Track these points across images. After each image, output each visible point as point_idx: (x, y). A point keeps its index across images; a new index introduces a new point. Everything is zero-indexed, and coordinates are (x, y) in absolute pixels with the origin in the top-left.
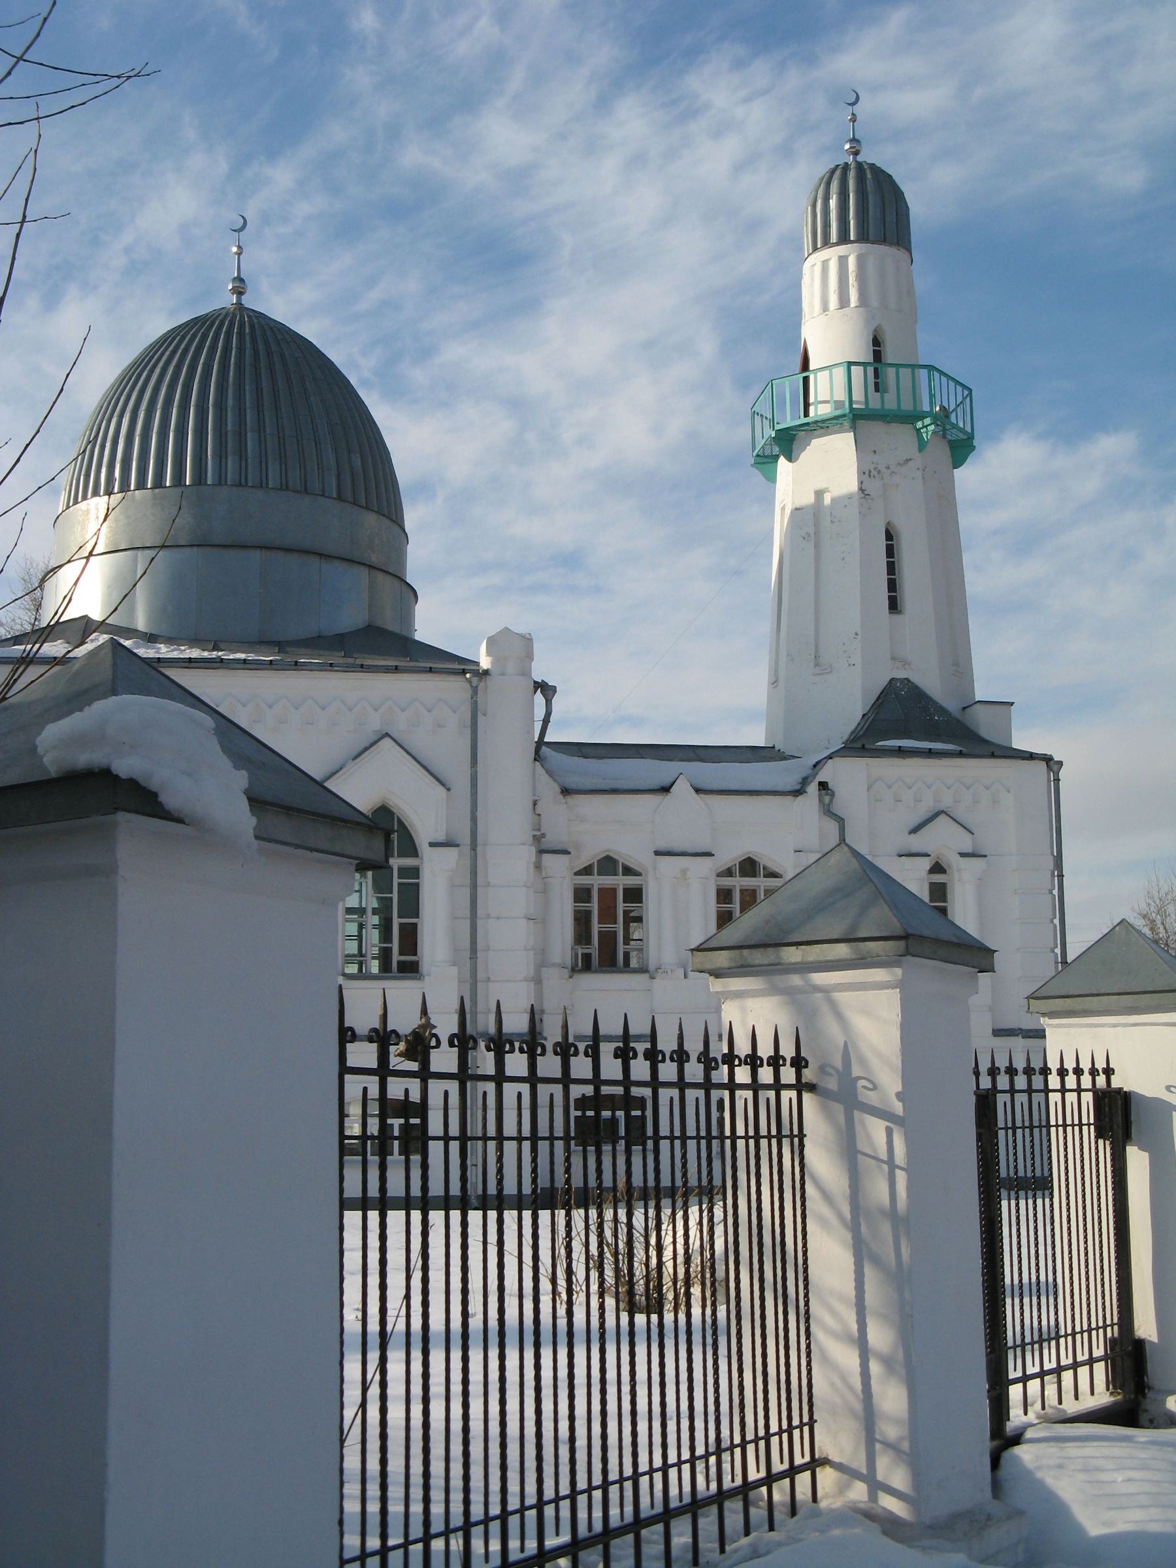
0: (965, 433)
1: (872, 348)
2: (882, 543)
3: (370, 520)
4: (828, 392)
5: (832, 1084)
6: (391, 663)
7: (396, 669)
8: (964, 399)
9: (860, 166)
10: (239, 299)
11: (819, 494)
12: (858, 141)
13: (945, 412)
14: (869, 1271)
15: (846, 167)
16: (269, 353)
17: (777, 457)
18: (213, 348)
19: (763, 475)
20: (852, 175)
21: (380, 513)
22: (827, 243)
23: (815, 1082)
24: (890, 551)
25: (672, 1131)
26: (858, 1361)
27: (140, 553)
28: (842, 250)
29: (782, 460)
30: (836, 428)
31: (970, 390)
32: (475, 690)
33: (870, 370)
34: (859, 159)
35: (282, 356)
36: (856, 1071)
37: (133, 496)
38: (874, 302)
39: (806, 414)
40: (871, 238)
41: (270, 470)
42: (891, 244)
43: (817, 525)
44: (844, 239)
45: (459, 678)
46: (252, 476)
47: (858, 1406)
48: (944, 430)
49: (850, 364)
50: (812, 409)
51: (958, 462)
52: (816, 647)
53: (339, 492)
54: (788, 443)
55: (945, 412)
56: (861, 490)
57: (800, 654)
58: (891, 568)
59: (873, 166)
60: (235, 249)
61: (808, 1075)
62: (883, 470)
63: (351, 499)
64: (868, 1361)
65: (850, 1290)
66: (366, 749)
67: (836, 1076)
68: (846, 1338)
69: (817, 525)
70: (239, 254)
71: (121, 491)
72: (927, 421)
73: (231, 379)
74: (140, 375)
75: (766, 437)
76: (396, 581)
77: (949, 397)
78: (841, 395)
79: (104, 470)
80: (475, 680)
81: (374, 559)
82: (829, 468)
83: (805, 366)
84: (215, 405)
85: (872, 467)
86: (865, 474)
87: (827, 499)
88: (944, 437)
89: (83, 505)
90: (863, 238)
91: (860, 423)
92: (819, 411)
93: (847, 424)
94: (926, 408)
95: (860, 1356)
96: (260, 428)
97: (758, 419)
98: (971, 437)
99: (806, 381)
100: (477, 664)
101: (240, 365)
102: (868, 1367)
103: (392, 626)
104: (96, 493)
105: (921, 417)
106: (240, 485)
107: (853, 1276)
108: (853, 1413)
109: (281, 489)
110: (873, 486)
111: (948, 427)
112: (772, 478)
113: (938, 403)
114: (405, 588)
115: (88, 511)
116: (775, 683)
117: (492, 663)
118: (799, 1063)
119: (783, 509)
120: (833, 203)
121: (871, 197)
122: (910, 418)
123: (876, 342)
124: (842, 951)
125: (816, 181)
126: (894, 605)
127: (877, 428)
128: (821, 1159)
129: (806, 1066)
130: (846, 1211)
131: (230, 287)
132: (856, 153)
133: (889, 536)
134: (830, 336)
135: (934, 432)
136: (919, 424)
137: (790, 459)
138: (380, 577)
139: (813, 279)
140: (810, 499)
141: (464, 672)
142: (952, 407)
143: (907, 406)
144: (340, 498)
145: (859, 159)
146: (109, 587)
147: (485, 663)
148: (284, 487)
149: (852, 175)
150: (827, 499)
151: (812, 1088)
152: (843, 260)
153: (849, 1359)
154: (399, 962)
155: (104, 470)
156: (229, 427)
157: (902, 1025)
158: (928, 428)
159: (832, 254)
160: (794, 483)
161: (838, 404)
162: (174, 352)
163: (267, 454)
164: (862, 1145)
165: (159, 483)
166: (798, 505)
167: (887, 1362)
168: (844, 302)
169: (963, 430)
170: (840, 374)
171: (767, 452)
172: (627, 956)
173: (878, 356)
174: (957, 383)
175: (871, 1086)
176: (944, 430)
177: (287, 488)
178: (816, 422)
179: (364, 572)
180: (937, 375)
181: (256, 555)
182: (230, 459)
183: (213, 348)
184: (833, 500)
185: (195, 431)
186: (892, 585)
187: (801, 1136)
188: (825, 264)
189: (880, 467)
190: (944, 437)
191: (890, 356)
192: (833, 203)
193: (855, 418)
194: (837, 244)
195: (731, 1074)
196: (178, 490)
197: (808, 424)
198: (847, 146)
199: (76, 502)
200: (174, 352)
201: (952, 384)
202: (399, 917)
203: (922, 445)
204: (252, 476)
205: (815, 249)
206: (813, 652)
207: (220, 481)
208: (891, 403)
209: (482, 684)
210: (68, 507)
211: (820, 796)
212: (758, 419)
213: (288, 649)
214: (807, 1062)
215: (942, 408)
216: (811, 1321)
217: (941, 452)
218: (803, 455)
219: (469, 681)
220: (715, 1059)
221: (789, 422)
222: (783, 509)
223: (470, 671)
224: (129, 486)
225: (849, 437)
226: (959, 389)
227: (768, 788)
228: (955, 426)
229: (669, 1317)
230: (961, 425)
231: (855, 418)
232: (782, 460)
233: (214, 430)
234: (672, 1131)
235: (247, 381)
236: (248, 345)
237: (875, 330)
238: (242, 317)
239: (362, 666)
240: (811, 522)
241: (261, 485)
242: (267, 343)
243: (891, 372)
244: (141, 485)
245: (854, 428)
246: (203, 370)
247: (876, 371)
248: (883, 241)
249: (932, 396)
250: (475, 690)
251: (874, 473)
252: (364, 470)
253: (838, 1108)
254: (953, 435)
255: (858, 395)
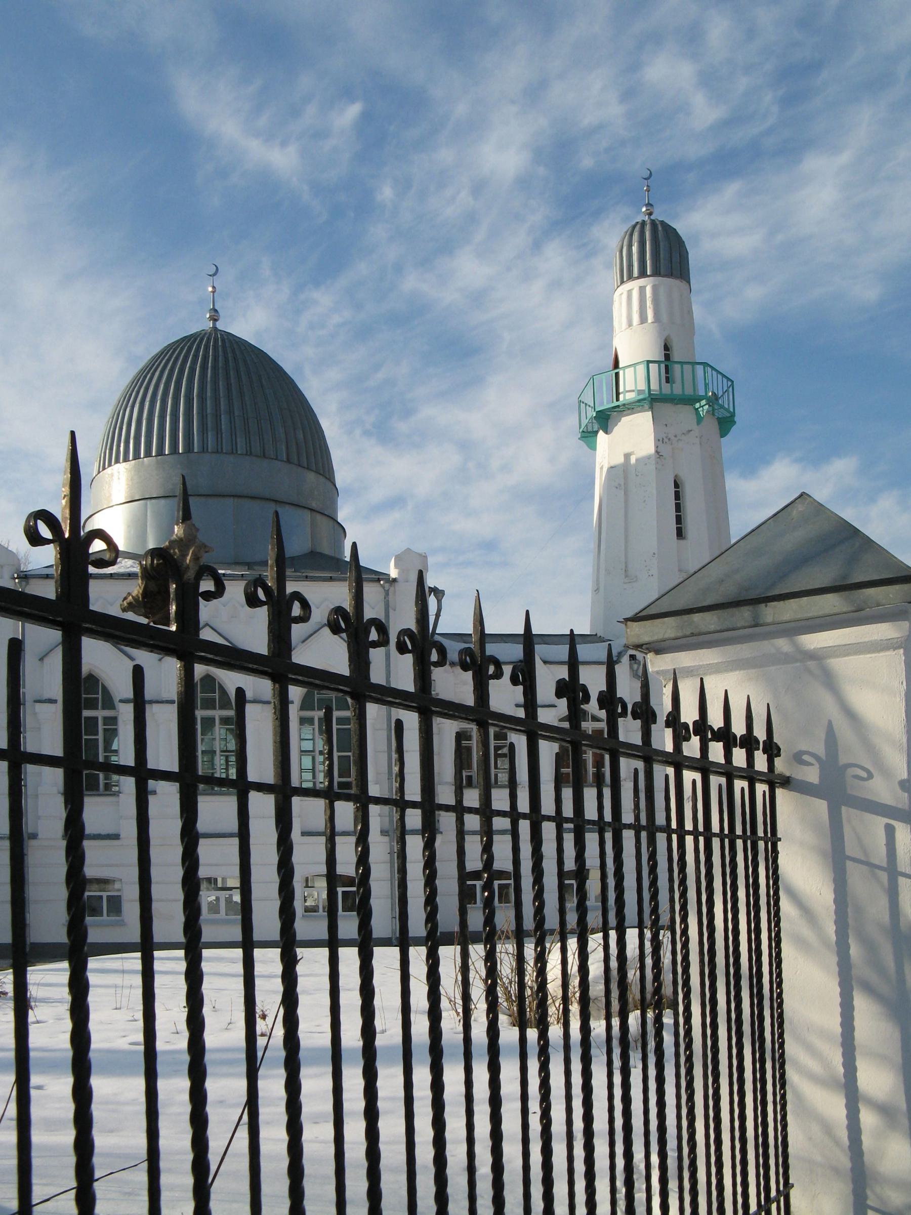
0: (729, 412)
1: (663, 352)
2: (672, 490)
3: (311, 476)
4: (633, 383)
5: (811, 775)
6: (327, 575)
7: (331, 579)
8: (728, 388)
9: (653, 223)
10: (214, 324)
11: (627, 456)
12: (651, 205)
13: (715, 397)
14: (861, 1004)
15: (643, 223)
16: (235, 359)
17: (597, 432)
18: (196, 356)
19: (588, 446)
20: (648, 229)
21: (317, 472)
22: (630, 277)
23: (788, 774)
24: (677, 496)
25: (637, 818)
26: (844, 1112)
27: (149, 502)
28: (642, 282)
29: (601, 433)
30: (639, 409)
31: (732, 382)
32: (387, 593)
33: (663, 366)
34: (652, 217)
35: (245, 361)
36: (843, 760)
37: (143, 462)
38: (665, 318)
39: (618, 400)
40: (662, 273)
41: (238, 440)
42: (676, 277)
43: (626, 478)
44: (643, 274)
45: (376, 584)
46: (226, 447)
47: (846, 1163)
48: (713, 410)
49: (649, 362)
50: (621, 397)
51: (723, 434)
52: (626, 563)
53: (288, 455)
54: (605, 420)
55: (715, 397)
56: (657, 452)
57: (614, 566)
58: (678, 508)
59: (662, 222)
60: (210, 289)
61: (780, 765)
62: (673, 438)
63: (296, 461)
64: (858, 1111)
65: (834, 1023)
66: (312, 635)
67: (817, 766)
68: (826, 1082)
69: (626, 478)
70: (213, 292)
71: (134, 459)
72: (703, 402)
73: (209, 379)
74: (145, 377)
75: (589, 417)
76: (331, 522)
77: (718, 385)
78: (642, 386)
79: (122, 445)
80: (387, 585)
81: (314, 505)
82: (635, 436)
83: (616, 364)
84: (198, 396)
85: (664, 436)
86: (660, 441)
87: (633, 460)
88: (713, 414)
89: (109, 471)
90: (656, 273)
91: (657, 405)
92: (627, 397)
93: (647, 406)
94: (701, 392)
95: (847, 1106)
96: (230, 412)
97: (583, 405)
98: (733, 415)
99: (617, 375)
100: (389, 575)
101: (215, 367)
102: (858, 1120)
103: (326, 549)
104: (117, 461)
105: (699, 401)
106: (217, 452)
107: (839, 1010)
108: (836, 1171)
109: (246, 454)
110: (666, 450)
111: (716, 407)
112: (593, 447)
113: (711, 389)
114: (337, 526)
115: (112, 475)
116: (597, 590)
117: (399, 574)
118: (772, 750)
119: (602, 468)
120: (635, 249)
121: (661, 244)
122: (690, 401)
123: (666, 348)
124: (831, 603)
125: (623, 233)
126: (680, 534)
127: (667, 409)
128: (802, 869)
129: (778, 755)
130: (830, 929)
131: (208, 316)
132: (650, 214)
133: (676, 485)
134: (633, 344)
135: (708, 412)
136: (697, 405)
137: (606, 432)
138: (319, 517)
139: (621, 304)
140: (621, 460)
141: (379, 580)
142: (720, 394)
143: (689, 391)
144: (289, 461)
145: (652, 217)
146: (129, 526)
147: (393, 573)
148: (249, 453)
149: (648, 229)
150: (633, 460)
151: (786, 782)
152: (642, 289)
153: (834, 1107)
154: (339, 783)
155: (122, 445)
156: (209, 411)
157: (906, 695)
158: (703, 408)
159: (634, 286)
160: (609, 450)
161: (640, 392)
162: (168, 360)
163: (231, 415)
164: (851, 848)
165: (160, 452)
166: (612, 464)
167: (884, 1110)
168: (643, 319)
169: (727, 410)
170: (641, 369)
171: (590, 429)
172: (496, 776)
173: (667, 357)
174: (724, 376)
175: (864, 775)
176: (713, 410)
177: (251, 454)
178: (624, 405)
179: (307, 515)
180: (709, 369)
181: (230, 501)
182: (209, 433)
183: (196, 356)
184: (637, 460)
185: (185, 414)
186: (679, 520)
187: (773, 839)
188: (630, 292)
189: (670, 436)
190: (713, 414)
191: (676, 356)
192: (635, 249)
193: (653, 401)
194: (638, 278)
195: (704, 749)
196: (176, 456)
197: (618, 406)
198: (644, 209)
199: (104, 469)
200: (168, 360)
201: (720, 377)
202: (338, 751)
203: (699, 420)
204: (226, 447)
205: (622, 282)
206: (623, 567)
207: (204, 449)
208: (677, 390)
209: (392, 589)
210: (99, 472)
211: (630, 665)
212: (583, 405)
213: (255, 568)
214: (779, 749)
215: (714, 393)
216: (787, 1067)
217: (712, 426)
218: (616, 429)
219: (382, 586)
220: (686, 726)
221: (606, 406)
222: (602, 468)
223: (383, 579)
224: (140, 454)
225: (649, 414)
226: (725, 380)
227: (594, 660)
228: (722, 407)
229: (555, 1032)
230: (726, 406)
231: (653, 401)
232: (601, 433)
233: (198, 413)
234: (637, 818)
235: (221, 379)
236: (221, 353)
237: (666, 340)
238: (216, 340)
239: (307, 577)
240: (622, 475)
241: (233, 452)
242: (233, 351)
243: (677, 367)
244: (148, 454)
245: (651, 408)
246: (189, 373)
247: (667, 368)
248: (670, 275)
249: (706, 385)
250: (387, 593)
251: (666, 440)
252: (305, 442)
253: (821, 806)
254: (722, 413)
255: (654, 386)
